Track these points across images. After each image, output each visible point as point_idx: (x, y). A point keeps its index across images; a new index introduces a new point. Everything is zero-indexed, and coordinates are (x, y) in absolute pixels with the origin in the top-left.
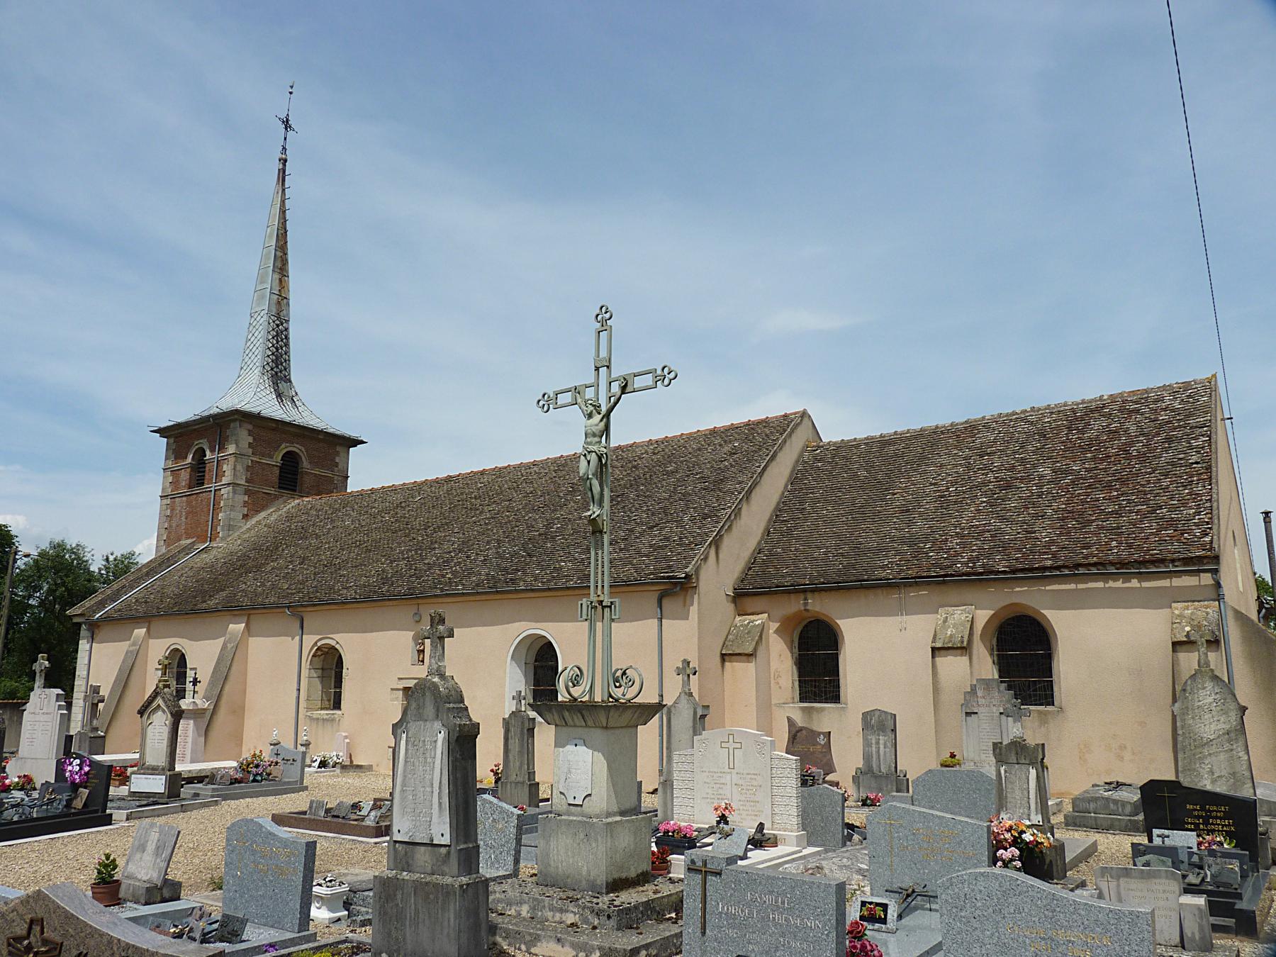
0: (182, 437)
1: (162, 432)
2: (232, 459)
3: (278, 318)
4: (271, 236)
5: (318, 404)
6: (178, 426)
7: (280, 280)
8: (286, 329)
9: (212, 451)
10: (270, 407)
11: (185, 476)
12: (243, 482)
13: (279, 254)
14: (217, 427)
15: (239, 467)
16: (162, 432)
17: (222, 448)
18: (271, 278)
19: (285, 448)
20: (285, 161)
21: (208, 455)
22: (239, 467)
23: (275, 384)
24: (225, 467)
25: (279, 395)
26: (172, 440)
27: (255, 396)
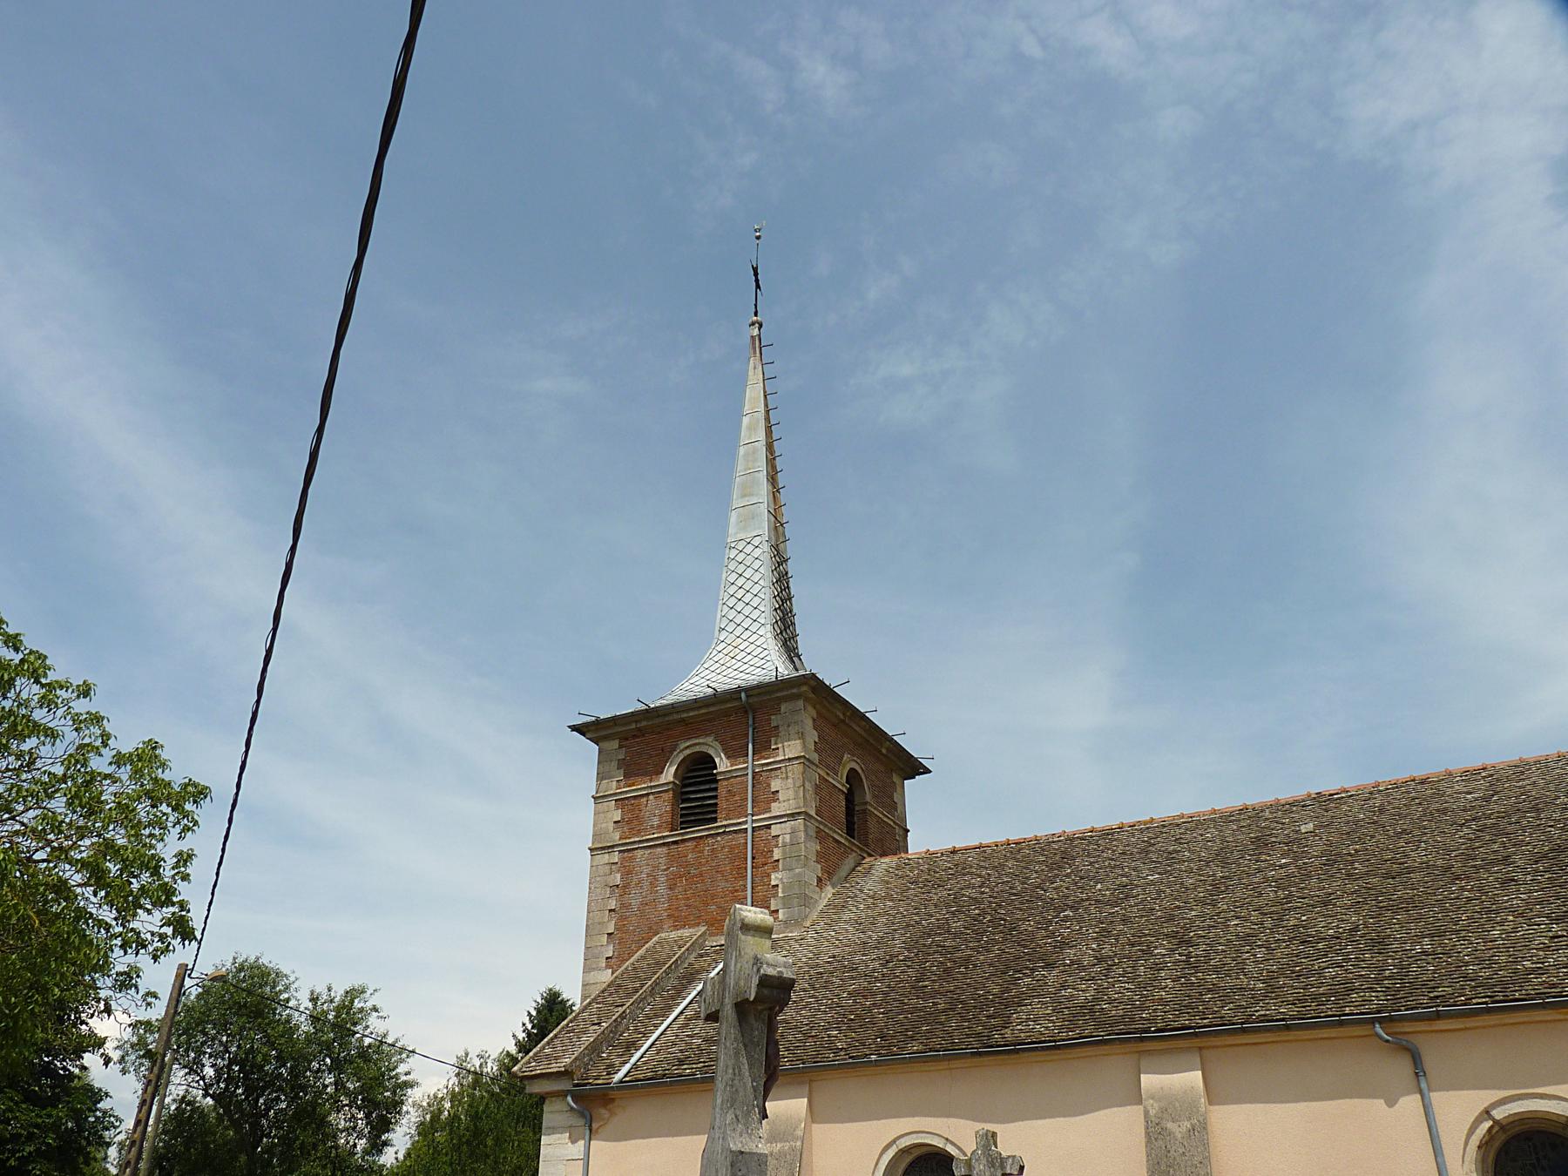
1: (591, 730)
2: (797, 768)
6: (649, 713)
9: (735, 753)
11: (658, 810)
12: (813, 813)
14: (746, 713)
16: (591, 730)
17: (762, 748)
21: (723, 764)
24: (775, 785)
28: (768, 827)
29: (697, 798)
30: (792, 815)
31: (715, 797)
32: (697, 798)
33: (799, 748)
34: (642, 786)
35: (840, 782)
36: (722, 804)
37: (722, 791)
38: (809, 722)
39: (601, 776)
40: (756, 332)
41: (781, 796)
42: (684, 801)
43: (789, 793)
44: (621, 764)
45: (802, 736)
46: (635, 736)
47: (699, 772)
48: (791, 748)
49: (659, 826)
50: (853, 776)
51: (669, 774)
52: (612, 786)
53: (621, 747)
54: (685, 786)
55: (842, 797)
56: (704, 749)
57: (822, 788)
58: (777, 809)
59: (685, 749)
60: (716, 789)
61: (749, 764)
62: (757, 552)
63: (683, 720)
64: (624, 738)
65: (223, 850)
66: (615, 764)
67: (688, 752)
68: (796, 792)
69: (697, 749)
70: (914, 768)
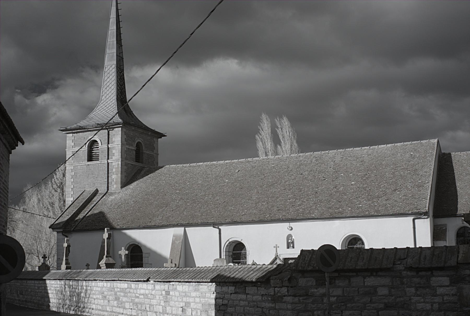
24: (114, 151)
35: (134, 148)
50: (138, 145)
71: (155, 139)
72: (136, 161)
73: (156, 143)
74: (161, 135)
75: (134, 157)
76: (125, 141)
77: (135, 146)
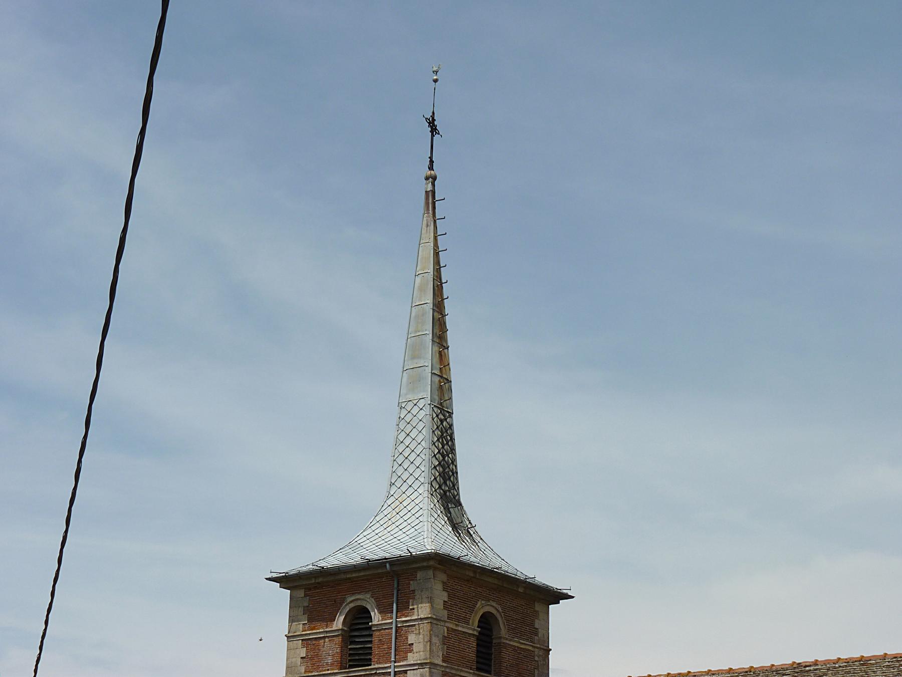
0: (315, 592)
1: (285, 581)
2: (425, 627)
3: (442, 410)
4: (422, 289)
5: (508, 543)
6: (323, 573)
7: (440, 353)
8: (451, 426)
9: (385, 610)
10: (453, 547)
11: (331, 650)
12: (439, 661)
13: (437, 316)
14: (394, 578)
15: (435, 640)
16: (285, 581)
17: (403, 608)
18: (429, 349)
19: (482, 607)
20: (435, 178)
21: (376, 618)
22: (435, 640)
23: (447, 510)
24: (412, 638)
25: (455, 527)
26: (301, 593)
27: (411, 529)
28: (405, 672)
29: (358, 644)
30: (421, 664)
31: (371, 642)
32: (358, 644)
33: (428, 610)
34: (320, 630)
35: (472, 628)
36: (376, 651)
37: (375, 639)
38: (439, 586)
39: (292, 619)
40: (430, 187)
41: (415, 648)
42: (352, 643)
43: (420, 646)
44: (306, 610)
45: (431, 600)
46: (315, 588)
47: (359, 617)
48: (422, 610)
49: (332, 664)
50: (487, 622)
51: (339, 623)
52: (299, 628)
53: (306, 595)
54: (352, 630)
55: (473, 639)
56: (364, 604)
57: (450, 641)
58: (412, 658)
59: (351, 601)
60: (371, 635)
61: (391, 620)
62: (422, 413)
63: (349, 579)
64: (308, 588)
65: (41, 648)
66: (301, 609)
67: (352, 605)
68: (425, 646)
69: (359, 603)
70: (557, 596)
71: (538, 607)
72: (478, 669)
73: (541, 615)
74: (557, 596)
75: (473, 656)
76: (445, 608)
77: (476, 623)
